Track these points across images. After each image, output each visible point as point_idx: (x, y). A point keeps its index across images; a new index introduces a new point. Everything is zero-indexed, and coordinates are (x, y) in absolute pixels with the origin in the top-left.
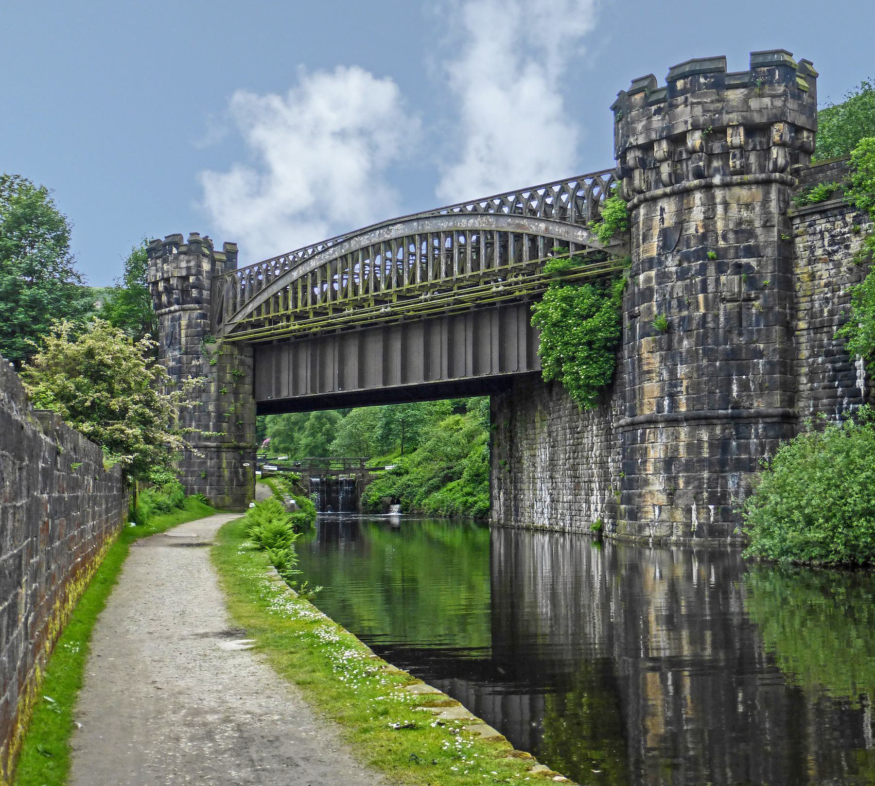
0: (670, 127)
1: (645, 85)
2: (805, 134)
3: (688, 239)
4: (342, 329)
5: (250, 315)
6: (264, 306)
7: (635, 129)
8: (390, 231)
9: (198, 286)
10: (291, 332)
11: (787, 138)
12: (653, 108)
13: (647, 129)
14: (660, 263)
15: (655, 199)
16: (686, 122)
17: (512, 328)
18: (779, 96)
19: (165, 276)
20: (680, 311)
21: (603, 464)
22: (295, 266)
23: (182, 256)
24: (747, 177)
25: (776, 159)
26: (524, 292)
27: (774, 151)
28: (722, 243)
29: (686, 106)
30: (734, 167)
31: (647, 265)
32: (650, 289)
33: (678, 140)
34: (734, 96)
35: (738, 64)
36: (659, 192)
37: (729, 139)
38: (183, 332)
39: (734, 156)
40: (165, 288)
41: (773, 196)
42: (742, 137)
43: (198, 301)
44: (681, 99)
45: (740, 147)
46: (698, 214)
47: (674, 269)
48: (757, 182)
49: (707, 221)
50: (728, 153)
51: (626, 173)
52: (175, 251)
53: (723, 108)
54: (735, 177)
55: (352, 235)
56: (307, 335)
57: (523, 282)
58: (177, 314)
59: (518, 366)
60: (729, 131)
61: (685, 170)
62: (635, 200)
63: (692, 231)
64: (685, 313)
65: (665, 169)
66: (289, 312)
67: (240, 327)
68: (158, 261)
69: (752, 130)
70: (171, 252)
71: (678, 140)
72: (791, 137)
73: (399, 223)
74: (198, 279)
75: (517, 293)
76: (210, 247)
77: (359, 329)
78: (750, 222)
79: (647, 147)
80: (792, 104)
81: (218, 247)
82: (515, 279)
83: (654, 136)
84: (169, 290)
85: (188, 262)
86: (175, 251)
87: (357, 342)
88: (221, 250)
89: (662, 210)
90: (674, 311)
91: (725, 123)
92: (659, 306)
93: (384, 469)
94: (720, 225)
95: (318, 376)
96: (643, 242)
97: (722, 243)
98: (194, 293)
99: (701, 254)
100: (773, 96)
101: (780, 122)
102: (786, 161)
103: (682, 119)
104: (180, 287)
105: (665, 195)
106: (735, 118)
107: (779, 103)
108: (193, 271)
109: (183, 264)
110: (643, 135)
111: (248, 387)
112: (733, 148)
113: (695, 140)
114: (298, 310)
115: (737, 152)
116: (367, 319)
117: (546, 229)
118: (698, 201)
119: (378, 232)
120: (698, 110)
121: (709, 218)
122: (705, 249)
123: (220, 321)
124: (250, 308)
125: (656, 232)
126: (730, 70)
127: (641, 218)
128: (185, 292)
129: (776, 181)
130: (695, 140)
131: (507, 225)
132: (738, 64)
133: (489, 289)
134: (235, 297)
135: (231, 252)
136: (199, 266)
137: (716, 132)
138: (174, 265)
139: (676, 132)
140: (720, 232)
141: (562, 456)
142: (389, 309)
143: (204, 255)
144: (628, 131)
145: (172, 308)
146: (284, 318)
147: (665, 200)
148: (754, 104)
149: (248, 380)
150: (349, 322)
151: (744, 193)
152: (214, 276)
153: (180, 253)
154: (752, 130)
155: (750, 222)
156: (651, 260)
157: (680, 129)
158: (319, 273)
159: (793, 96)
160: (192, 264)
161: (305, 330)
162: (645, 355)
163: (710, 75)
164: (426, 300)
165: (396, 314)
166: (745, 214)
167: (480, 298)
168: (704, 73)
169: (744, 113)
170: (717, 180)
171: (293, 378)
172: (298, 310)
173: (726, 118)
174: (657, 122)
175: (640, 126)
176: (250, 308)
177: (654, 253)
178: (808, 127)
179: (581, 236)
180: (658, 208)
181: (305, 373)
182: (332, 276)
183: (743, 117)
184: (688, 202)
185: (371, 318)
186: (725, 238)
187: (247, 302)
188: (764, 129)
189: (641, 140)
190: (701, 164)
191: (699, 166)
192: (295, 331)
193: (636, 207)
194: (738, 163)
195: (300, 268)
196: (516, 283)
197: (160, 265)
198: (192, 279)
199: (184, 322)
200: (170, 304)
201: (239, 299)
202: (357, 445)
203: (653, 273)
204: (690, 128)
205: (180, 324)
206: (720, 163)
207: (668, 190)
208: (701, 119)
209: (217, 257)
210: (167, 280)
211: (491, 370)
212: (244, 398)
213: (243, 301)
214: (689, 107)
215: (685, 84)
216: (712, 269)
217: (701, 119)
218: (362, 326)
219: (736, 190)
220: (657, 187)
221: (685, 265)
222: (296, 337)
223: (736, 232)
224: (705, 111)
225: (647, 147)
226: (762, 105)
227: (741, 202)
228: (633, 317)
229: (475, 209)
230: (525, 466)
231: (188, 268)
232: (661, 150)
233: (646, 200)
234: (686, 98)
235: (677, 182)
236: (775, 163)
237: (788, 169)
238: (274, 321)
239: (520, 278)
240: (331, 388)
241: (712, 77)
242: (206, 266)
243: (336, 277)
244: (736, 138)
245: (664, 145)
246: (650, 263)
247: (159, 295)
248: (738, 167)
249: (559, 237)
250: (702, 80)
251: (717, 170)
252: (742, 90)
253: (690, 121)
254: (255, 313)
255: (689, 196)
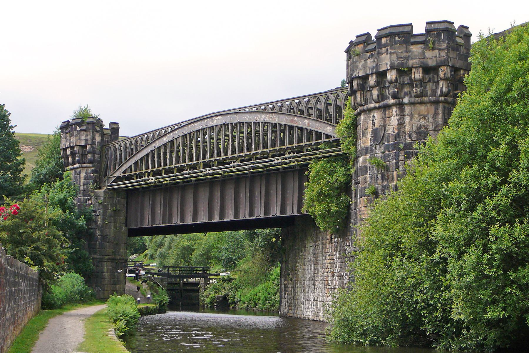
0: (377, 66)
1: (364, 39)
2: (462, 72)
3: (388, 136)
4: (183, 182)
5: (125, 172)
6: (163, 147)
7: (357, 66)
8: (214, 120)
9: (93, 152)
10: (150, 183)
11: (449, 75)
12: (368, 54)
13: (365, 67)
14: (372, 151)
15: (370, 110)
16: (387, 64)
17: (290, 186)
18: (443, 50)
19: (72, 145)
20: (383, 182)
21: (341, 277)
22: (161, 137)
23: (83, 132)
24: (425, 99)
25: (442, 88)
26: (296, 163)
27: (441, 83)
28: (408, 140)
29: (387, 54)
30: (416, 92)
31: (364, 151)
32: (366, 167)
33: (382, 75)
34: (416, 49)
35: (419, 29)
36: (373, 105)
37: (413, 76)
38: (82, 182)
39: (416, 86)
40: (71, 152)
41: (440, 111)
42: (421, 74)
43: (90, 162)
44: (384, 50)
45: (420, 80)
46: (394, 121)
47: (380, 155)
48: (431, 103)
49: (399, 126)
50: (413, 84)
51: (353, 93)
52: (78, 129)
53: (409, 56)
54: (417, 99)
55: (190, 122)
56: (161, 185)
57: (294, 157)
58: (79, 170)
59: (292, 211)
60: (413, 70)
61: (387, 93)
62: (358, 110)
63: (391, 131)
64: (385, 183)
65: (375, 93)
66: (149, 171)
67: (119, 179)
68: (67, 135)
69: (427, 70)
70: (76, 130)
71: (382, 75)
72: (451, 75)
73: (219, 115)
74: (92, 147)
75: (292, 164)
76: (101, 126)
77: (193, 182)
78: (426, 127)
79: (365, 78)
80: (452, 55)
81: (106, 126)
82: (289, 155)
83: (368, 72)
84: (73, 154)
85: (86, 136)
86: (78, 129)
87: (193, 191)
88: (108, 127)
89: (374, 117)
90: (379, 181)
91: (410, 66)
92: (371, 178)
93: (219, 275)
94: (407, 129)
95: (168, 214)
96: (363, 136)
97: (408, 140)
98: (90, 157)
99: (395, 147)
100: (440, 50)
101: (444, 66)
102: (449, 89)
103: (385, 62)
104: (81, 153)
105: (375, 108)
106: (415, 62)
107: (443, 54)
108: (90, 143)
109: (83, 138)
110: (362, 71)
111: (122, 219)
112: (415, 81)
113: (392, 76)
114: (155, 169)
115: (418, 83)
116: (198, 176)
117: (308, 124)
118: (394, 113)
119: (206, 121)
120: (394, 57)
121: (401, 124)
122: (398, 144)
123: (106, 175)
124: (124, 168)
125: (370, 131)
126: (415, 32)
127: (362, 122)
128: (83, 155)
129: (442, 102)
130: (392, 76)
131: (285, 120)
132: (419, 29)
133: (273, 161)
134: (116, 159)
135: (115, 128)
136: (93, 138)
137: (403, 71)
138: (77, 138)
139: (381, 70)
140: (407, 133)
141: (320, 270)
142: (211, 172)
143: (97, 131)
144: (353, 67)
145: (75, 166)
146: (147, 174)
147: (376, 111)
148: (429, 54)
149: (123, 214)
150: (187, 178)
151: (423, 109)
152: (103, 144)
153: (81, 130)
154: (427, 70)
155: (426, 127)
156: (366, 148)
157: (383, 69)
158: (168, 146)
159: (453, 49)
160: (89, 137)
161: (159, 182)
162: (362, 209)
163: (400, 34)
164: (234, 167)
165: (216, 174)
166: (423, 122)
167: (270, 166)
168: (398, 34)
169: (422, 60)
170: (406, 100)
171: (151, 215)
172: (155, 169)
173: (411, 62)
174: (370, 63)
175: (360, 65)
176: (124, 168)
177: (368, 144)
178: (463, 68)
179: (328, 130)
180: (372, 116)
181: (159, 211)
182: (197, 138)
183: (421, 62)
184: (389, 114)
185: (201, 176)
186: (410, 137)
187: (123, 162)
188: (434, 70)
189: (361, 74)
190: (396, 90)
191: (394, 92)
192: (152, 183)
193: (359, 114)
194: (418, 90)
195: (157, 142)
196: (290, 158)
197: (68, 138)
198: (88, 147)
199: (83, 175)
200: (74, 163)
201: (118, 161)
202: (207, 257)
203: (368, 157)
204: (389, 68)
205: (80, 177)
206: (409, 90)
207: (377, 105)
208: (396, 63)
209: (105, 131)
210: (72, 148)
211: (276, 212)
212: (120, 226)
213: (120, 163)
214: (389, 55)
215: (387, 41)
216: (402, 157)
217: (396, 63)
218: (196, 180)
219: (418, 107)
220: (371, 103)
221: (387, 152)
222: (154, 186)
223: (417, 133)
224: (398, 58)
225: (365, 78)
226: (432, 57)
227: (421, 114)
228: (357, 183)
229: (265, 109)
230: (300, 277)
231: (86, 140)
232: (372, 80)
233: (364, 111)
234: (387, 50)
235: (383, 101)
236: (441, 91)
237: (451, 94)
238: (140, 176)
239: (292, 155)
240: (176, 221)
241: (402, 37)
242: (98, 138)
243: (199, 139)
244: (417, 75)
245: (374, 77)
246: (366, 151)
247: (67, 157)
248: (419, 92)
249: (316, 130)
250: (397, 39)
251: (406, 94)
252: (422, 45)
253: (389, 64)
254: (128, 171)
255: (389, 109)
